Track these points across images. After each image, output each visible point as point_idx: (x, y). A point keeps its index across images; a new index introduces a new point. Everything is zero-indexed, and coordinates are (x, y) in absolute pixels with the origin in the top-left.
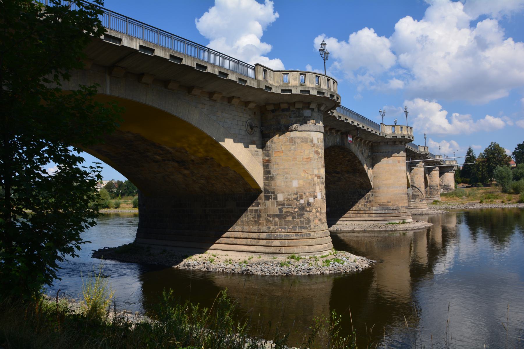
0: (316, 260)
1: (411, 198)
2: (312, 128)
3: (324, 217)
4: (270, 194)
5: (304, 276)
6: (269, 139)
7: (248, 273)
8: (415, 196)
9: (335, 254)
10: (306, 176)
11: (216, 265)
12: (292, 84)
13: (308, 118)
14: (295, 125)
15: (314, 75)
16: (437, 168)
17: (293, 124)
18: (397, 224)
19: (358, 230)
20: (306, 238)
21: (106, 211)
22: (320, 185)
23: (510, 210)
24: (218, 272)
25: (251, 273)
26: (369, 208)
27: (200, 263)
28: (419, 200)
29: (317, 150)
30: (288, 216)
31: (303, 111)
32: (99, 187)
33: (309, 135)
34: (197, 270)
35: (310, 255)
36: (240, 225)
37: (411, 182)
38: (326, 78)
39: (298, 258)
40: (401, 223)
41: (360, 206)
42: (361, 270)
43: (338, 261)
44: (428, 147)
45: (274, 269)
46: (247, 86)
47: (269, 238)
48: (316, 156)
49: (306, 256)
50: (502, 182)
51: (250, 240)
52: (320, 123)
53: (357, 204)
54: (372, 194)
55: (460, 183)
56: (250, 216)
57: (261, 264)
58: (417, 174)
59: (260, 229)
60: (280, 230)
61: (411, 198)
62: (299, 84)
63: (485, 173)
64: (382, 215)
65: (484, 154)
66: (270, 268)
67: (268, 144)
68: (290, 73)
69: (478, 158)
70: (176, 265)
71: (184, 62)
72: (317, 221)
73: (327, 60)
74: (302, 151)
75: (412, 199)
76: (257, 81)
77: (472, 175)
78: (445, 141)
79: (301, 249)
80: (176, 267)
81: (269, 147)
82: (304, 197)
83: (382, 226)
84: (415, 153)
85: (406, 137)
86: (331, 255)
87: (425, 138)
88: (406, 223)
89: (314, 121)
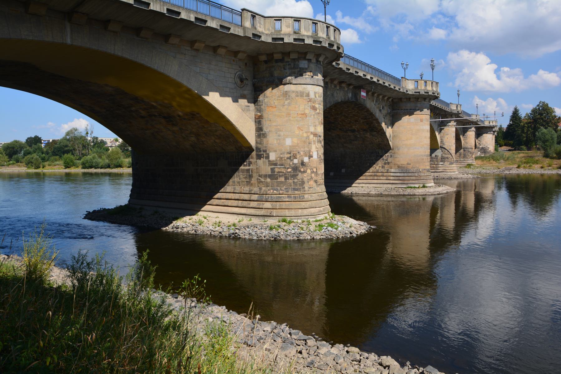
0: (309, 223)
1: (439, 160)
2: (309, 81)
3: (321, 178)
4: (262, 153)
5: (294, 240)
6: (262, 93)
7: (236, 236)
8: (444, 158)
9: (331, 219)
10: (301, 134)
11: (204, 228)
12: (285, 31)
13: (305, 70)
14: (289, 78)
15: (310, 22)
16: (473, 129)
17: (288, 77)
18: (416, 188)
19: (373, 193)
20: (299, 200)
21: (118, 170)
22: (317, 143)
23: (550, 176)
24: (206, 235)
25: (238, 236)
26: (388, 170)
27: (189, 225)
28: (449, 163)
29: (313, 105)
30: (280, 176)
31: (299, 62)
32: (114, 145)
33: (304, 88)
34: (185, 233)
35: (303, 219)
36: (231, 185)
37: (441, 144)
38: (325, 25)
39: (290, 221)
40: (421, 187)
41: (377, 168)
42: (355, 236)
43: (331, 225)
44: (461, 105)
45: (262, 233)
46: (231, 33)
47: (261, 200)
48: (313, 112)
49: (299, 220)
50: (545, 145)
51: (241, 201)
52: (318, 76)
53: (374, 165)
54: (391, 155)
55: (503, 146)
56: (241, 176)
57: (250, 227)
58: (448, 134)
59: (252, 190)
60: (272, 191)
61: (439, 160)
62: (293, 31)
63: (530, 135)
64: (401, 178)
65: (531, 114)
66: (258, 232)
67: (261, 98)
68: (282, 19)
69: (523, 119)
70: (165, 227)
71: (152, 7)
72: (312, 183)
73: (328, 4)
74: (297, 107)
75: (441, 161)
76: (243, 28)
77: (516, 137)
78: (491, 99)
79: (293, 213)
80: (164, 229)
81: (261, 101)
82: (298, 156)
83: (400, 190)
84: (445, 111)
85: (430, 93)
86: (326, 219)
87: (458, 95)
88: (426, 187)
89: (312, 73)
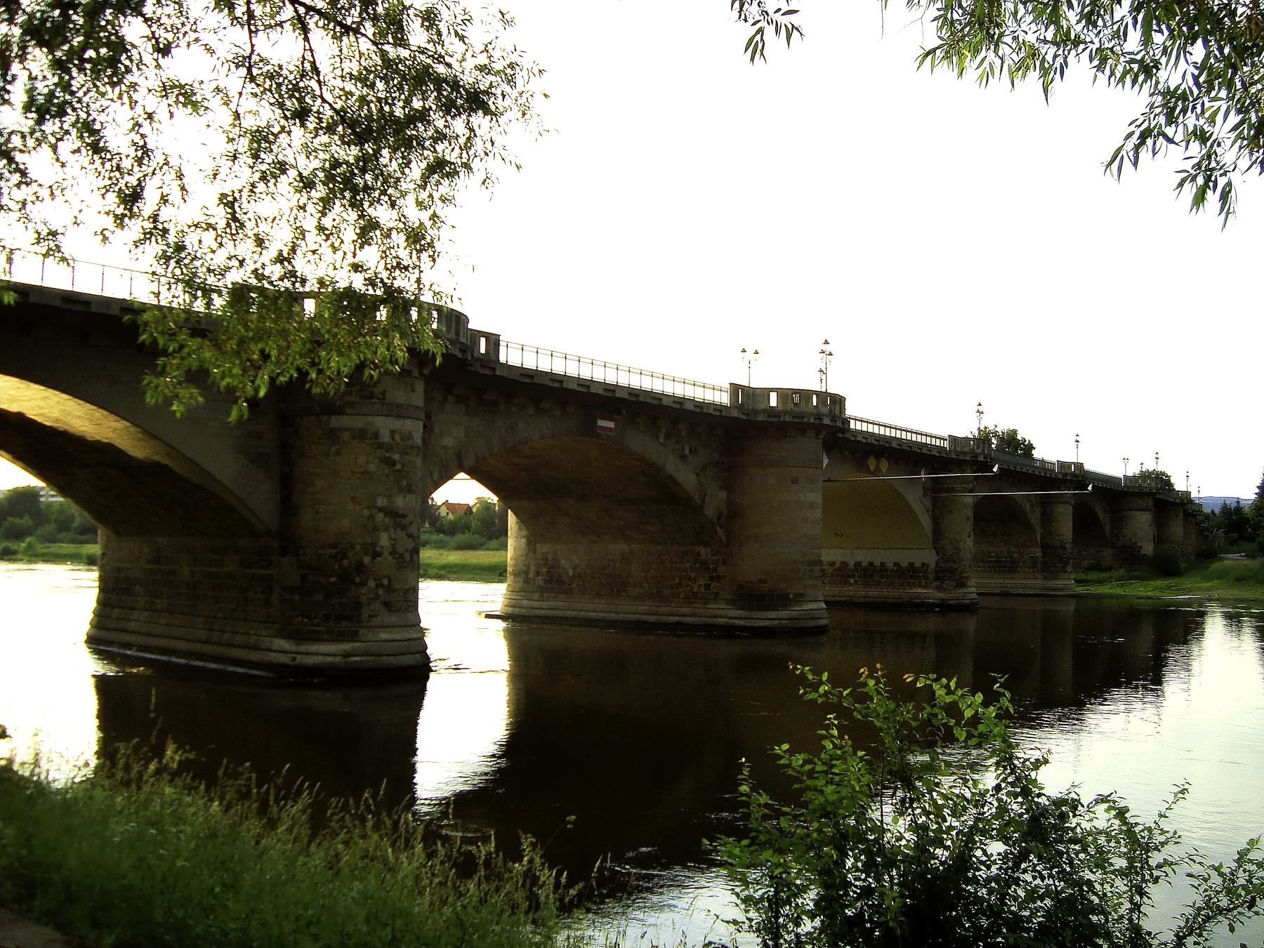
1: (931, 576)
22: (392, 530)
29: (387, 455)
33: (368, 423)
82: (350, 554)
